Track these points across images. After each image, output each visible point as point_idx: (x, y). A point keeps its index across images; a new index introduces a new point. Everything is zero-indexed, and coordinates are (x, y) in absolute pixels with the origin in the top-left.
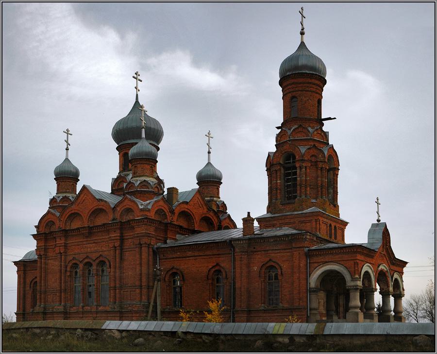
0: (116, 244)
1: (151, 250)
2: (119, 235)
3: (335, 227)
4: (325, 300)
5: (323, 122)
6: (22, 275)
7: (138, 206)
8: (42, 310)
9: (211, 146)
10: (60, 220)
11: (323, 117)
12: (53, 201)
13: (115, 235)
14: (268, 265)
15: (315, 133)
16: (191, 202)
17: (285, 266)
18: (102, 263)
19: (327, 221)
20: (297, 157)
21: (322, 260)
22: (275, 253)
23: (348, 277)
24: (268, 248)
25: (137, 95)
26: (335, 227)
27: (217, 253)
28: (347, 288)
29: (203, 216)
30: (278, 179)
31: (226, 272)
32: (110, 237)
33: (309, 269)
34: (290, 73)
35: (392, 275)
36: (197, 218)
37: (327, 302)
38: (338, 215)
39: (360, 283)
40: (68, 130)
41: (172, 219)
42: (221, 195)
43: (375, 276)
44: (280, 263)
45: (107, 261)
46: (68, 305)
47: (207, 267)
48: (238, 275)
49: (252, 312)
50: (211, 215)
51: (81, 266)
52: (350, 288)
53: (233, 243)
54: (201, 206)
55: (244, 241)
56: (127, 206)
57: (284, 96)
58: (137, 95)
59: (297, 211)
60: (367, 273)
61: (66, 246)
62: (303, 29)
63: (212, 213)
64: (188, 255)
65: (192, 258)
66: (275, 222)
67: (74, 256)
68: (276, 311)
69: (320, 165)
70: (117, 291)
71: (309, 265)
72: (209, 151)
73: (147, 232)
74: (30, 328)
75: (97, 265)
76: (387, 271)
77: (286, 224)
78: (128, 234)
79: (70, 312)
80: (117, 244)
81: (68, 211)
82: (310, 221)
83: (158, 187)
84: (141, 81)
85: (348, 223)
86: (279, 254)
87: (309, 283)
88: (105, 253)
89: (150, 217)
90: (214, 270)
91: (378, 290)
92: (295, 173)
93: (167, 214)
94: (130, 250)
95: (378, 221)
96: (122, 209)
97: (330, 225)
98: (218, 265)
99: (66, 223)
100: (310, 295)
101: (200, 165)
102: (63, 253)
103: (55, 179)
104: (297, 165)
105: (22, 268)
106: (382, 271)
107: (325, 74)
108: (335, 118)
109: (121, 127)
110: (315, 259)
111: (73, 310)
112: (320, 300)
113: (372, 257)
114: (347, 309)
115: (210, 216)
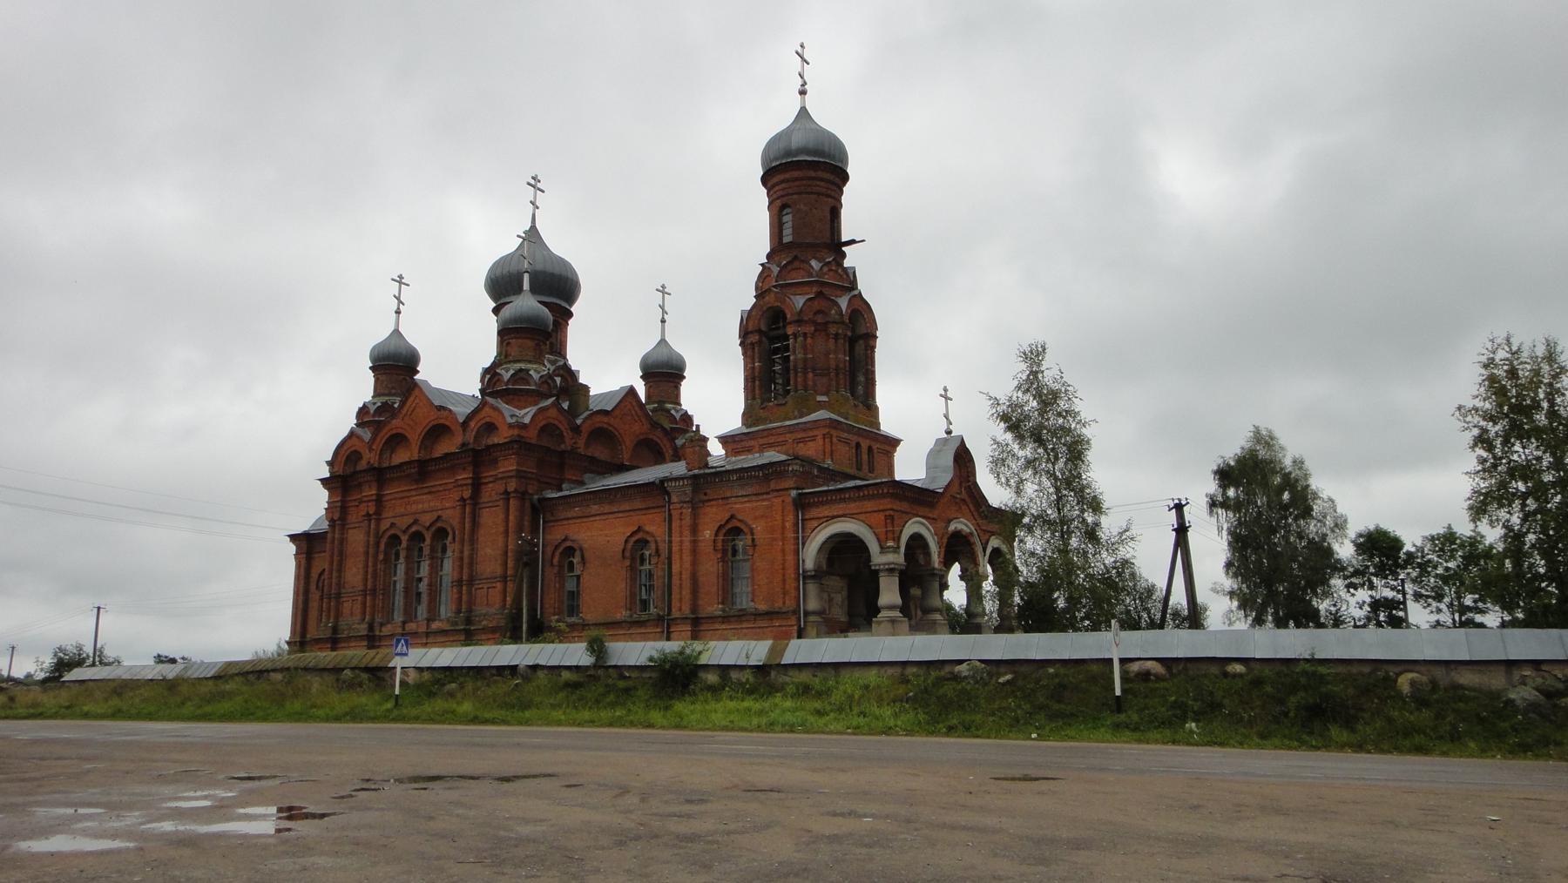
0: (465, 492)
1: (527, 504)
2: (471, 476)
3: (870, 449)
4: (845, 593)
5: (843, 249)
6: (303, 562)
7: (504, 418)
8: (328, 634)
9: (666, 309)
10: (371, 450)
11: (844, 239)
12: (363, 411)
13: (465, 476)
14: (729, 526)
15: (825, 269)
16: (617, 412)
17: (759, 527)
18: (441, 534)
19: (850, 436)
20: (788, 316)
21: (826, 513)
22: (742, 503)
23: (873, 547)
24: (729, 495)
25: (534, 216)
26: (870, 449)
27: (644, 507)
28: (873, 568)
29: (641, 437)
30: (757, 360)
31: (656, 542)
32: (457, 480)
33: (802, 532)
34: (778, 163)
35: (984, 542)
36: (629, 443)
37: (849, 597)
38: (877, 425)
39: (899, 559)
40: (401, 277)
41: (575, 443)
42: (683, 401)
43: (939, 544)
44: (750, 523)
45: (449, 530)
46: (378, 619)
47: (624, 533)
48: (675, 548)
49: (703, 621)
50: (657, 436)
51: (404, 538)
52: (877, 568)
53: (666, 485)
54: (636, 418)
55: (685, 481)
56: (488, 420)
57: (771, 203)
58: (534, 216)
59: (790, 419)
60: (917, 539)
61: (379, 501)
62: (804, 84)
63: (659, 433)
64: (593, 512)
65: (597, 518)
66: (752, 443)
67: (392, 520)
68: (744, 619)
69: (832, 330)
70: (464, 588)
71: (803, 524)
72: (663, 318)
73: (521, 469)
74: (265, 671)
75: (434, 537)
76: (971, 534)
77: (771, 446)
78: (488, 474)
79: (379, 636)
80: (467, 494)
81: (384, 431)
82: (813, 439)
83: (550, 381)
84: (543, 191)
85: (902, 440)
86: (747, 505)
87: (803, 561)
88: (448, 511)
89: (528, 441)
90: (634, 539)
91: (991, 578)
92: (787, 348)
93: (565, 434)
94: (490, 504)
95: (949, 432)
96: (479, 424)
97: (858, 445)
98: (639, 529)
99: (381, 454)
100: (804, 584)
101: (648, 344)
102: (374, 514)
103: (370, 368)
104: (790, 330)
105: (304, 546)
106: (957, 535)
107: (846, 163)
108: (863, 241)
109: (498, 272)
110: (814, 512)
111: (386, 630)
112: (832, 595)
113: (932, 505)
114: (874, 610)
115: (655, 438)
